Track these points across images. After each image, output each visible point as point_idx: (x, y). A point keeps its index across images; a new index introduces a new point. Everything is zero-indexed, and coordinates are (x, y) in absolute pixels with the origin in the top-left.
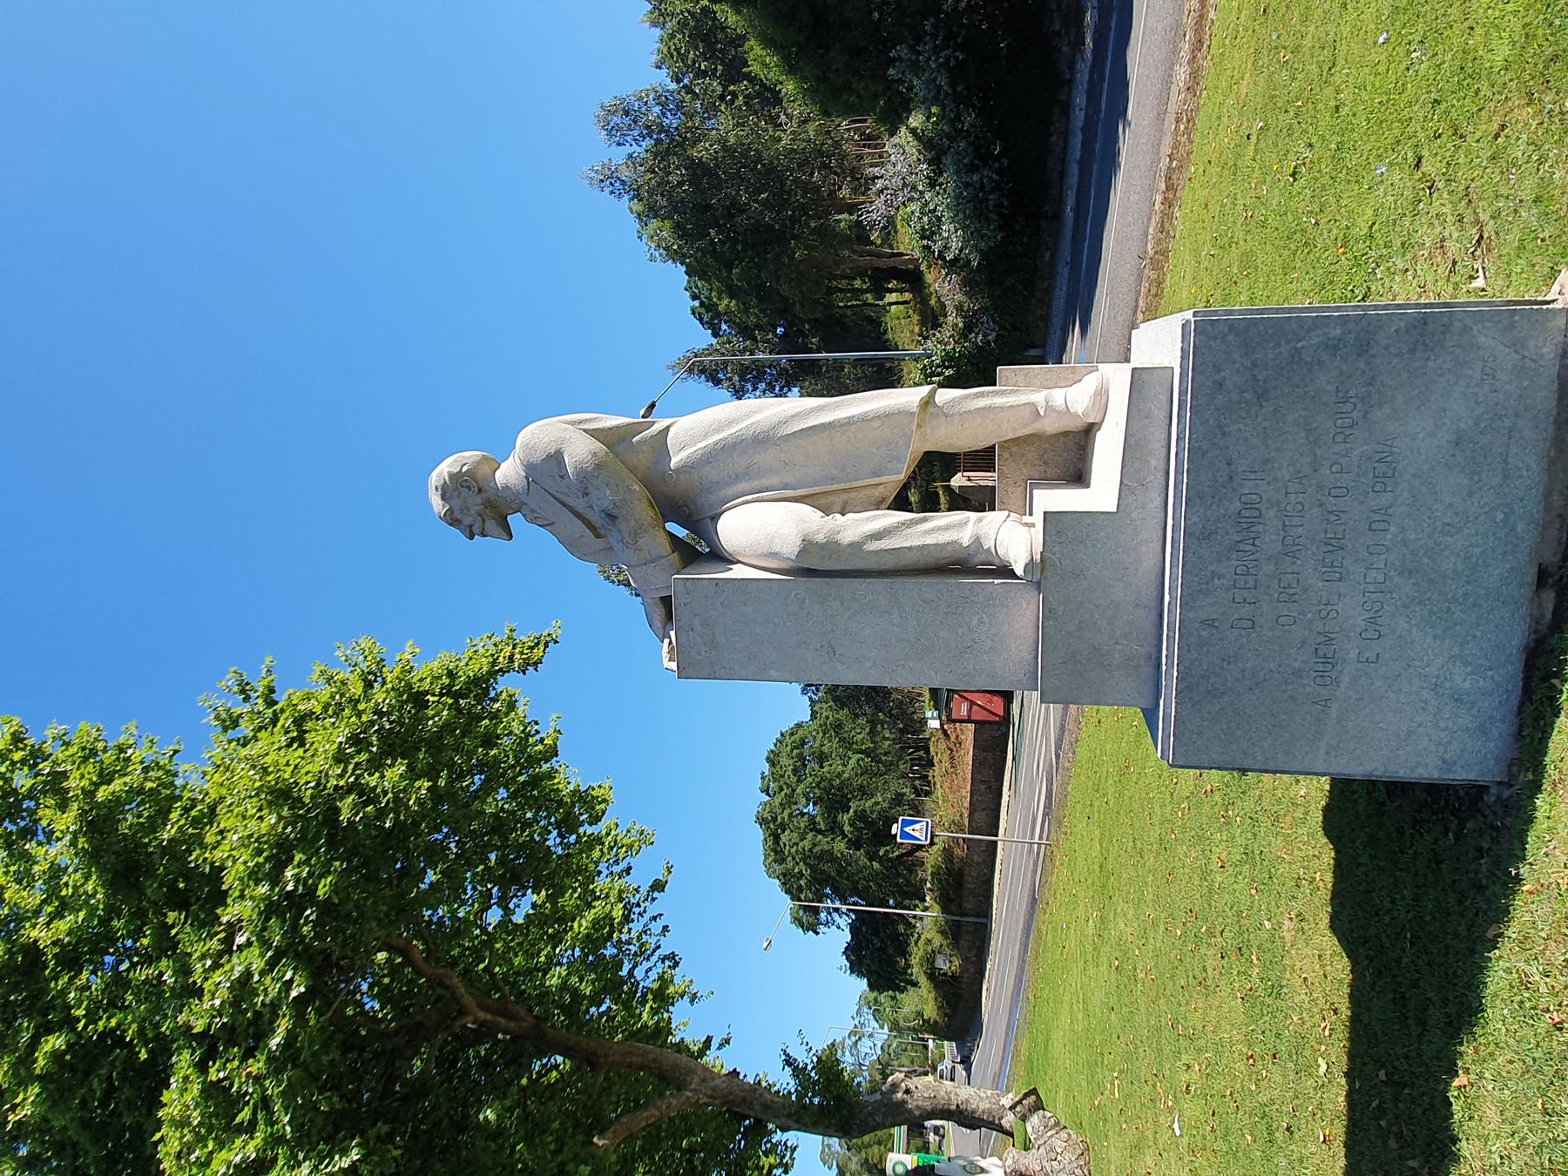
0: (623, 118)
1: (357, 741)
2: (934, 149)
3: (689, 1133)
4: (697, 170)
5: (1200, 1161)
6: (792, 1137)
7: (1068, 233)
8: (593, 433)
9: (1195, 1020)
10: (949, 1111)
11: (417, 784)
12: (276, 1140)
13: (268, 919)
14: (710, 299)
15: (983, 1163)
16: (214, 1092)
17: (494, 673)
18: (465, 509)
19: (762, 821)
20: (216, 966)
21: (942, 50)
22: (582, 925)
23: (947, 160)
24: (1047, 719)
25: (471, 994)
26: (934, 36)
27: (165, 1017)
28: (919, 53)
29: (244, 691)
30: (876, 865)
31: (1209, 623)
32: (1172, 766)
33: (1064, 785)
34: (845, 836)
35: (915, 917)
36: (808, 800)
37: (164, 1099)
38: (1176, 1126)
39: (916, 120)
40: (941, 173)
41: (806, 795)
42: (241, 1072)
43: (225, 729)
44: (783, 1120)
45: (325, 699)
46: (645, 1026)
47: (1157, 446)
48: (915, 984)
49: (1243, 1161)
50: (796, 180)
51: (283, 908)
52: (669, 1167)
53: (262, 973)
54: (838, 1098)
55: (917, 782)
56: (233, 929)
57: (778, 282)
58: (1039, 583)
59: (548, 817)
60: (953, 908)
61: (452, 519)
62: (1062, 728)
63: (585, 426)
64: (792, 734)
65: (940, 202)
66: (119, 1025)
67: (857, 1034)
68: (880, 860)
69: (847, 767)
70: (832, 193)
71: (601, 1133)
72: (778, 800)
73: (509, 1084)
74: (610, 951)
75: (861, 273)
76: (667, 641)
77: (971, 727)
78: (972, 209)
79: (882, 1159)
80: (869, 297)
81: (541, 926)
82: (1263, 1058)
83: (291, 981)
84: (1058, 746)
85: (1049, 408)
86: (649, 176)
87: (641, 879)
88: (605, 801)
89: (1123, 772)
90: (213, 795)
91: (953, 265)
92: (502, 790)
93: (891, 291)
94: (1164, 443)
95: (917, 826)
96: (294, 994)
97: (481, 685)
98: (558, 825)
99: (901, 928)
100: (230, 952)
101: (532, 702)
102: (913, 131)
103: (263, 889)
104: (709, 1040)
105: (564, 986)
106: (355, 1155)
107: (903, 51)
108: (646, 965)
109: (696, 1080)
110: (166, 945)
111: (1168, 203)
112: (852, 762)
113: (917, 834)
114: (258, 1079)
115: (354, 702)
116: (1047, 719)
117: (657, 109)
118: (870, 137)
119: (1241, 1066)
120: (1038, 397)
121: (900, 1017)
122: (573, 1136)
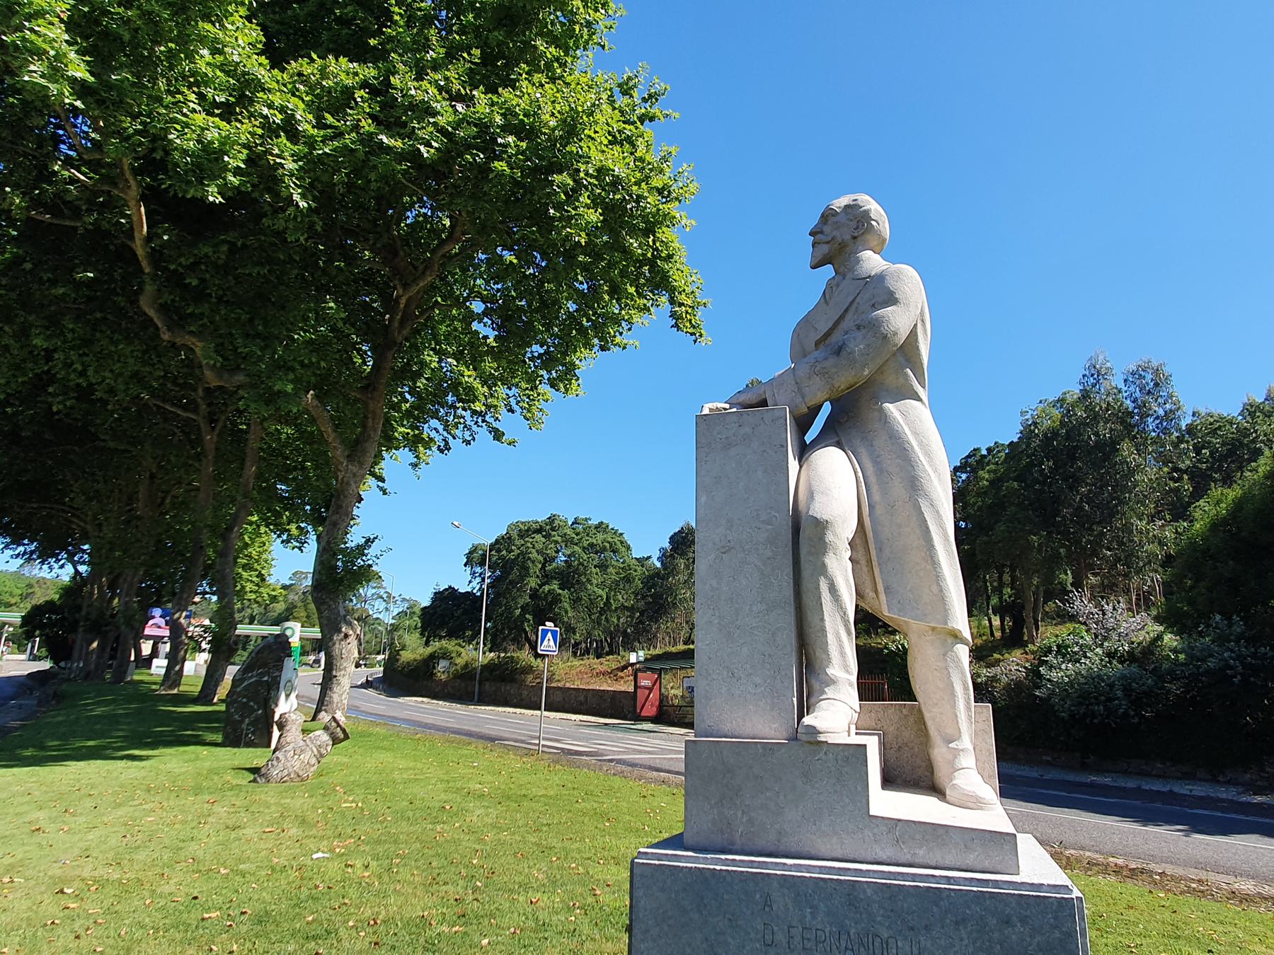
0: (1152, 382)
1: (616, 183)
2: (1144, 655)
3: (316, 467)
4: (1108, 448)
5: (294, 875)
6: (312, 546)
7: (1070, 777)
8: (913, 333)
9: (404, 874)
10: (331, 670)
11: (583, 234)
12: (311, 143)
13: (476, 125)
14: (988, 464)
15: (293, 696)
16: (348, 93)
17: (672, 291)
18: (837, 226)
19: (552, 519)
20: (440, 89)
21: (1241, 663)
22: (469, 376)
23: (1134, 668)
24: (640, 752)
25: (418, 292)
26: (1254, 656)
27: (400, 55)
28: (1237, 642)
29: (651, 98)
30: (518, 612)
31: (768, 902)
32: (632, 861)
33: (588, 766)
34: (540, 586)
35: (478, 643)
36: (569, 556)
37: (341, 59)
38: (320, 855)
39: (1170, 640)
40: (1121, 662)
41: (573, 554)
42: (362, 116)
43: (620, 85)
44: (325, 539)
45: (648, 158)
46: (394, 430)
47: (936, 857)
48: (427, 644)
49: (292, 913)
50: (1102, 534)
51: (486, 139)
52: (291, 452)
53: (435, 124)
54: (341, 581)
55: (583, 645)
56: (468, 100)
57: (1039, 506)
58: (796, 739)
59: (555, 345)
60: (486, 674)
61: (828, 215)
62: (633, 765)
63: (919, 325)
64: (622, 542)
65: (1094, 660)
66: (395, 23)
67: (389, 598)
68: (522, 615)
69: (596, 587)
70: (1091, 567)
71: (316, 396)
72: (569, 531)
73: (353, 325)
74: (450, 398)
75: (1019, 593)
76: (727, 406)
77: (631, 689)
78: (1088, 692)
79: (295, 619)
80: (994, 601)
81: (471, 344)
82: (375, 933)
83: (432, 147)
84: (619, 761)
85: (956, 753)
86: (1104, 406)
87: (506, 421)
88: (567, 390)
89: (604, 816)
90: (569, 79)
91: (1034, 673)
92: (575, 307)
93: (1002, 621)
94: (941, 863)
95: (552, 643)
96: (422, 148)
97: (661, 282)
98: (547, 352)
99: (469, 633)
100: (451, 98)
101: (647, 325)
102: (1159, 637)
103: (498, 119)
104: (383, 481)
105: (423, 364)
106: (303, 204)
107: (1239, 627)
108: (441, 428)
109: (355, 469)
110: (452, 54)
111: (1118, 871)
112: (600, 592)
113: (545, 643)
114: (356, 127)
115: (647, 179)
116: (640, 752)
117: (1161, 412)
118: (1147, 600)
119: (368, 913)
120: (966, 742)
121: (401, 632)
122: (315, 375)
